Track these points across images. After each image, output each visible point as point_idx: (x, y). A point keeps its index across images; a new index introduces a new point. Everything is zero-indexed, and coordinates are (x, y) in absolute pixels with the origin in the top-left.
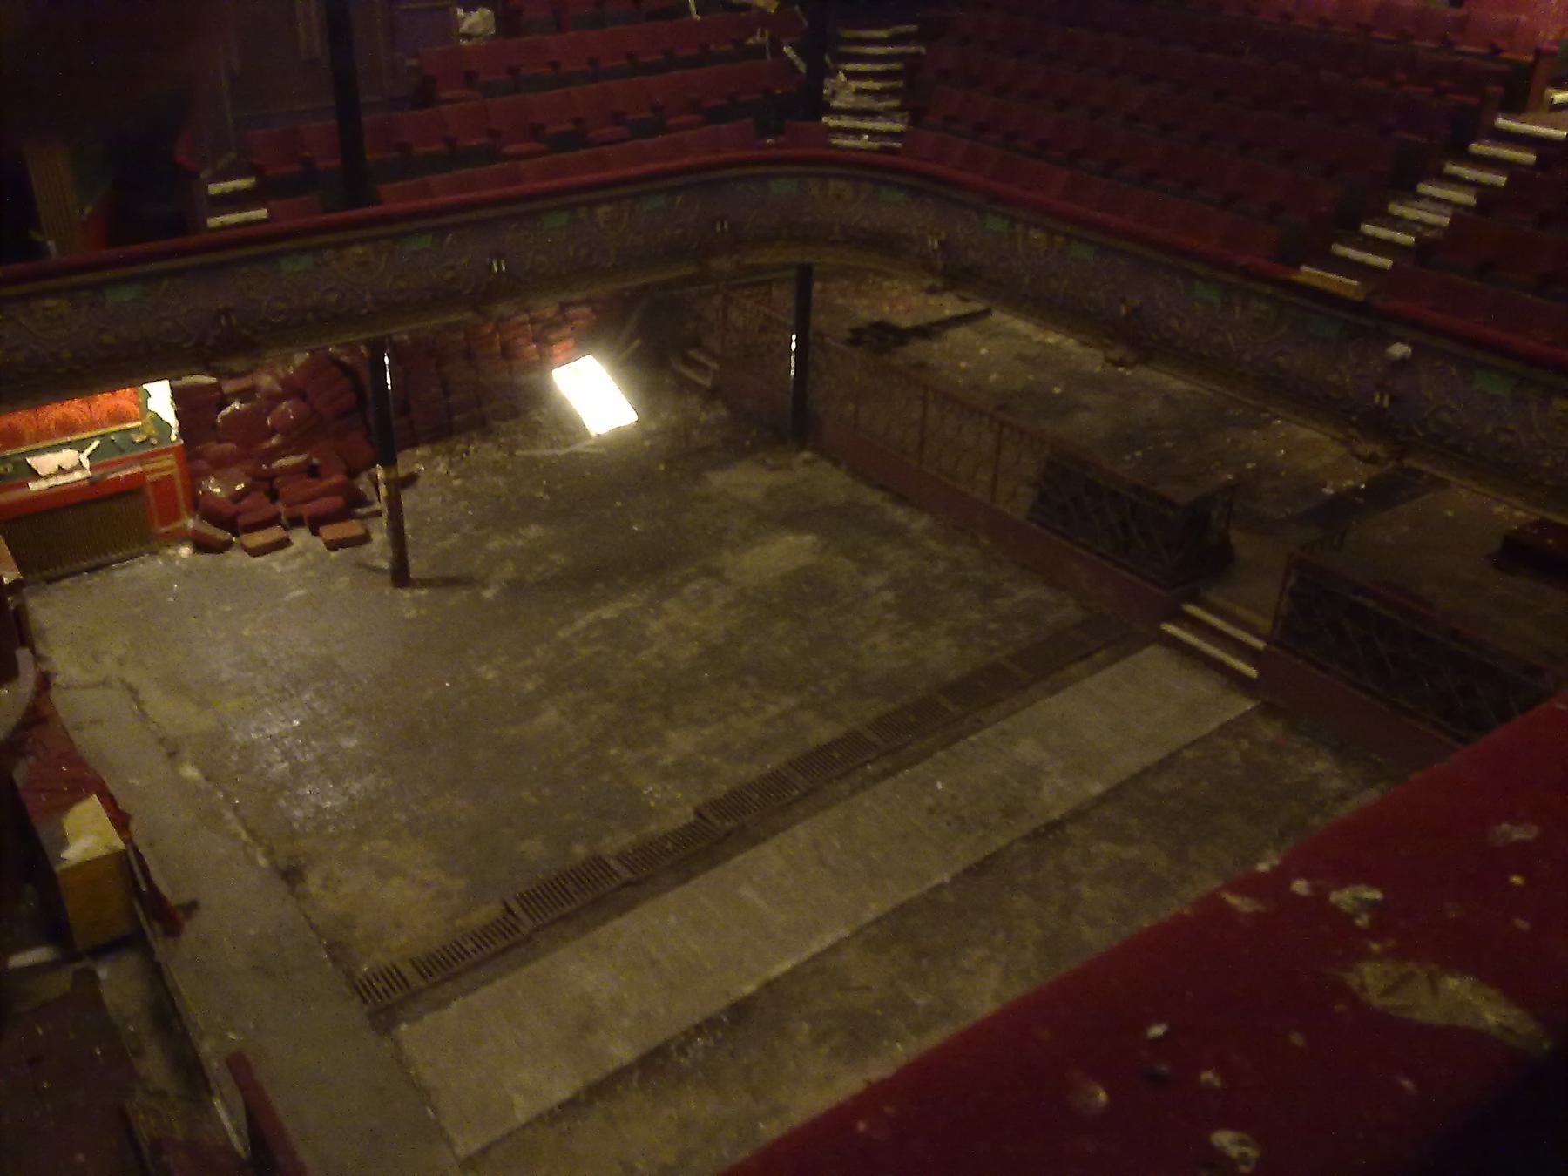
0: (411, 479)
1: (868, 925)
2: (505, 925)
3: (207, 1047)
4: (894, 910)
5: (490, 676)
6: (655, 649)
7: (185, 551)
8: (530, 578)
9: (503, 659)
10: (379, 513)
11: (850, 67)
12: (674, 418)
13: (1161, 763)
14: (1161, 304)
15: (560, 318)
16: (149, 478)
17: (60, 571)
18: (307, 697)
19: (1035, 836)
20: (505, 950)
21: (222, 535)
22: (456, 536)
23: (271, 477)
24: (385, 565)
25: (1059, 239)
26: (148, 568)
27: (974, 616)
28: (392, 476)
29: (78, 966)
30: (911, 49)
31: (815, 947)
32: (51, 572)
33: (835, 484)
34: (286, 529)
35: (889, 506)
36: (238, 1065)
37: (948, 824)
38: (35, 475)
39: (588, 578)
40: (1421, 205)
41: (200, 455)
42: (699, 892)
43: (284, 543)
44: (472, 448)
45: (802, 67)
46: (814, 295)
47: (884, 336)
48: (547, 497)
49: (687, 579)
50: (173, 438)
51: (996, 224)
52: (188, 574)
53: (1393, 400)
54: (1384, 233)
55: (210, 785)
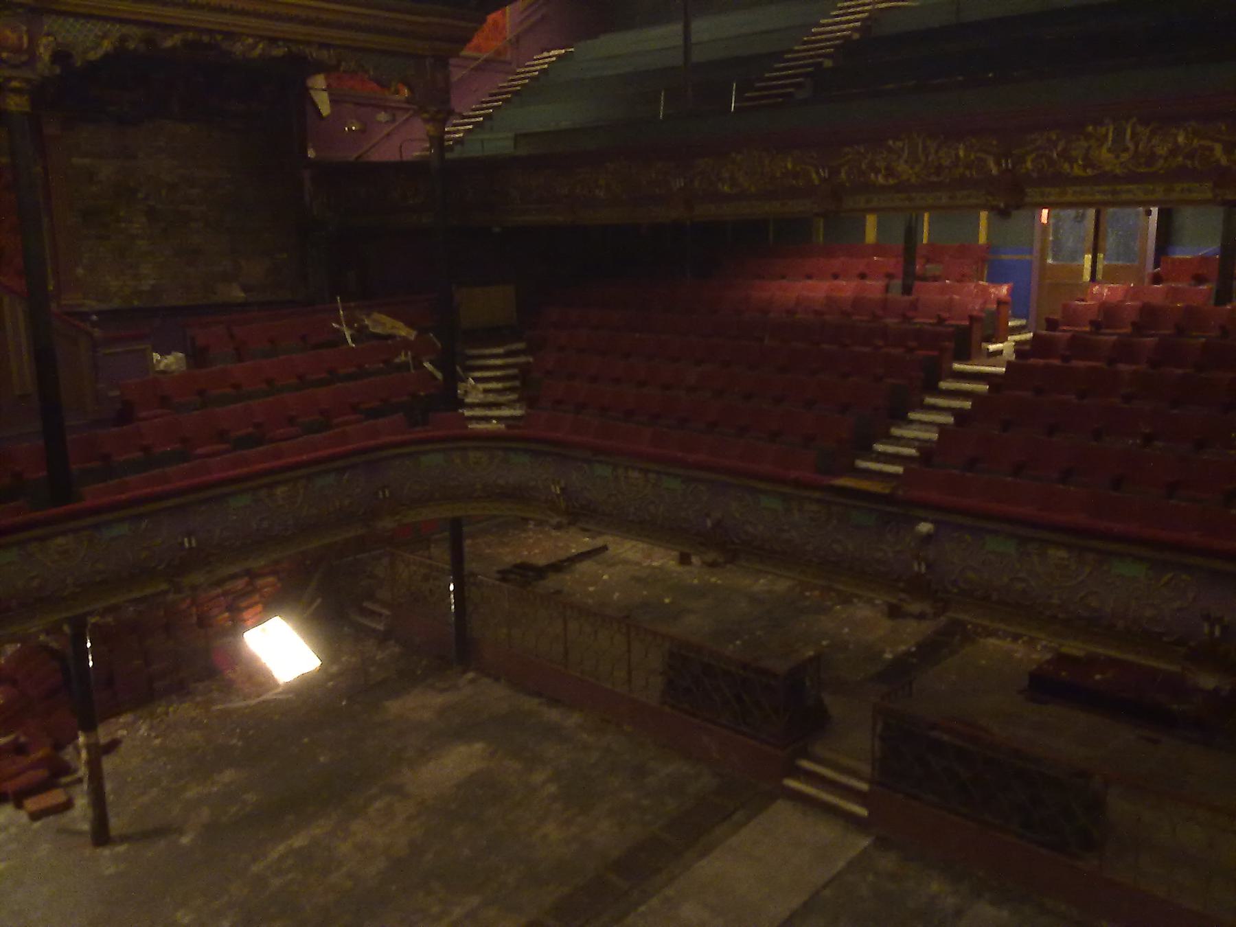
0: (113, 745)
6: (344, 869)
10: (80, 781)
11: (478, 374)
13: (805, 904)
14: (737, 515)
15: (250, 588)
24: (86, 827)
25: (652, 476)
30: (522, 359)
40: (914, 427)
44: (171, 709)
45: (439, 375)
46: (466, 550)
47: (526, 574)
51: (603, 471)
53: (928, 566)
54: (891, 449)
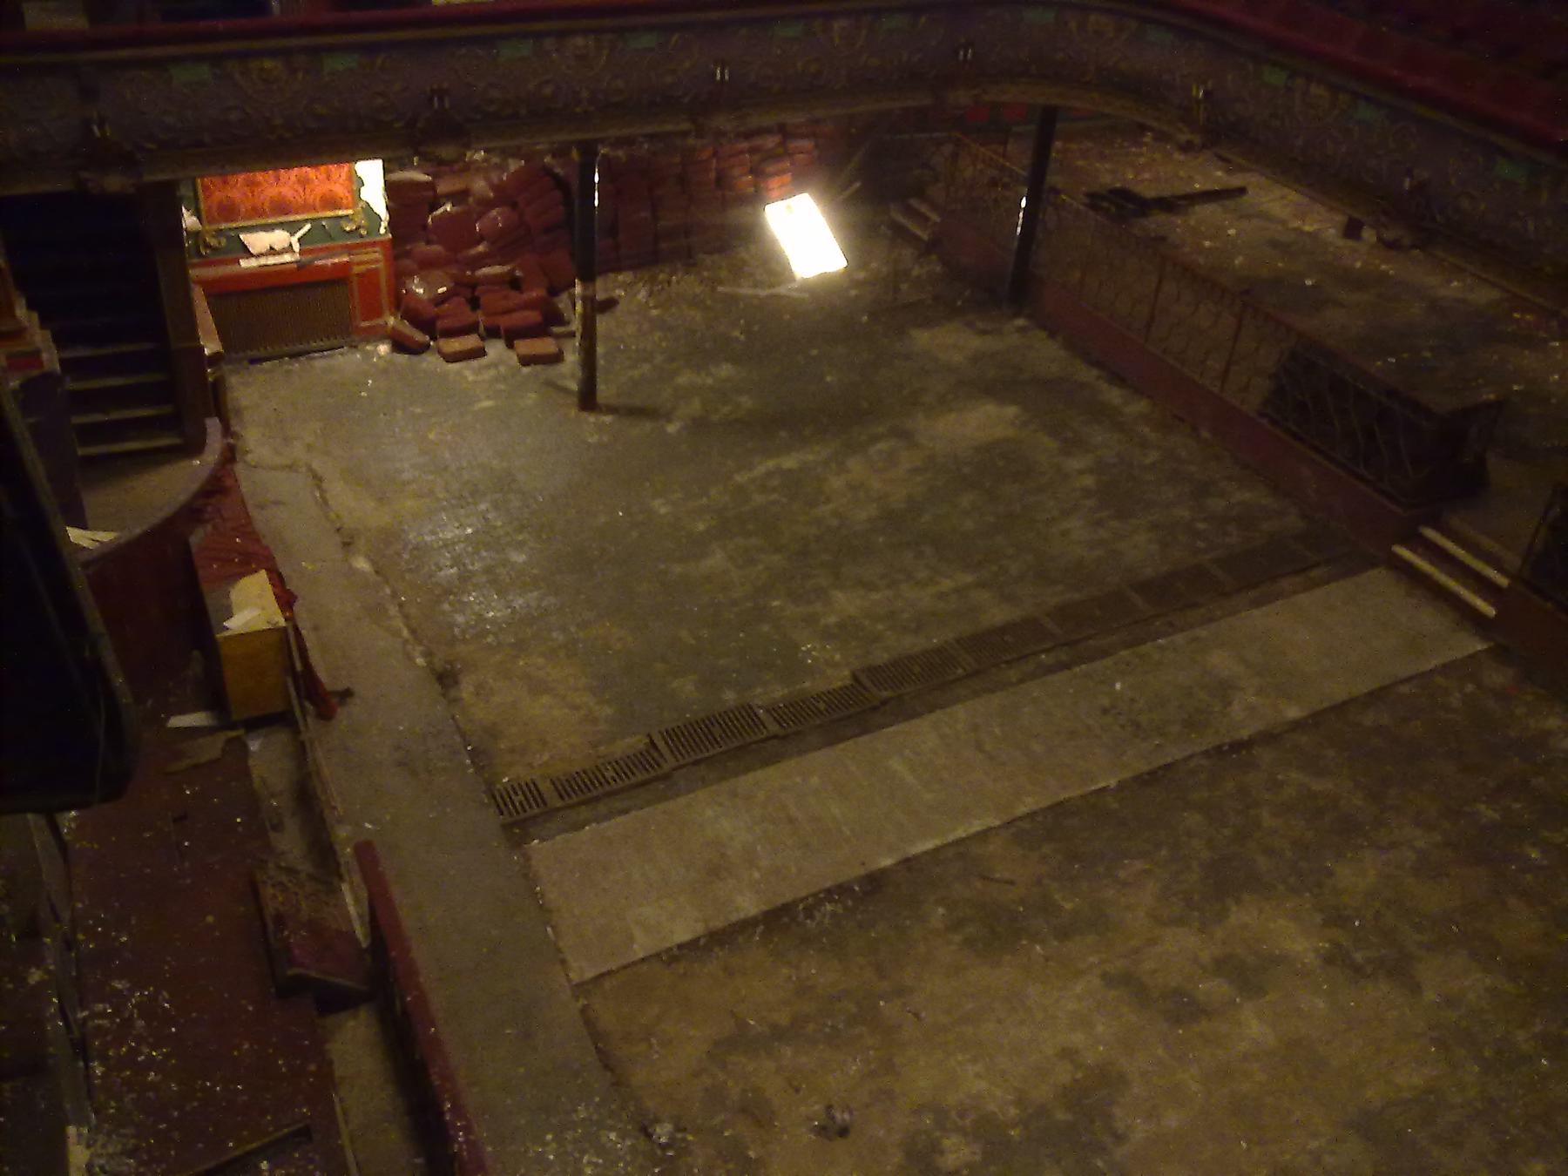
0: (609, 305)
1: (1021, 818)
2: (648, 757)
3: (342, 833)
4: (1050, 808)
5: (663, 511)
7: (383, 349)
8: (715, 418)
9: (679, 495)
10: (572, 335)
12: (884, 269)
13: (1371, 694)
15: (781, 150)
16: (357, 269)
17: (262, 353)
18: (483, 507)
19: (1218, 752)
20: (644, 784)
21: (420, 337)
22: (646, 367)
23: (473, 285)
24: (574, 386)
26: (346, 361)
27: (1183, 513)
28: (589, 293)
29: (233, 734)
31: (961, 833)
32: (254, 353)
33: (1046, 355)
34: (483, 339)
35: (1105, 386)
36: (365, 852)
37: (1123, 727)
38: (249, 254)
39: (776, 424)
41: (408, 254)
42: (849, 756)
43: (479, 353)
47: (1124, 205)
48: (742, 337)
49: (875, 439)
50: (382, 231)
51: (1276, 78)
52: (385, 371)
55: (379, 579)
